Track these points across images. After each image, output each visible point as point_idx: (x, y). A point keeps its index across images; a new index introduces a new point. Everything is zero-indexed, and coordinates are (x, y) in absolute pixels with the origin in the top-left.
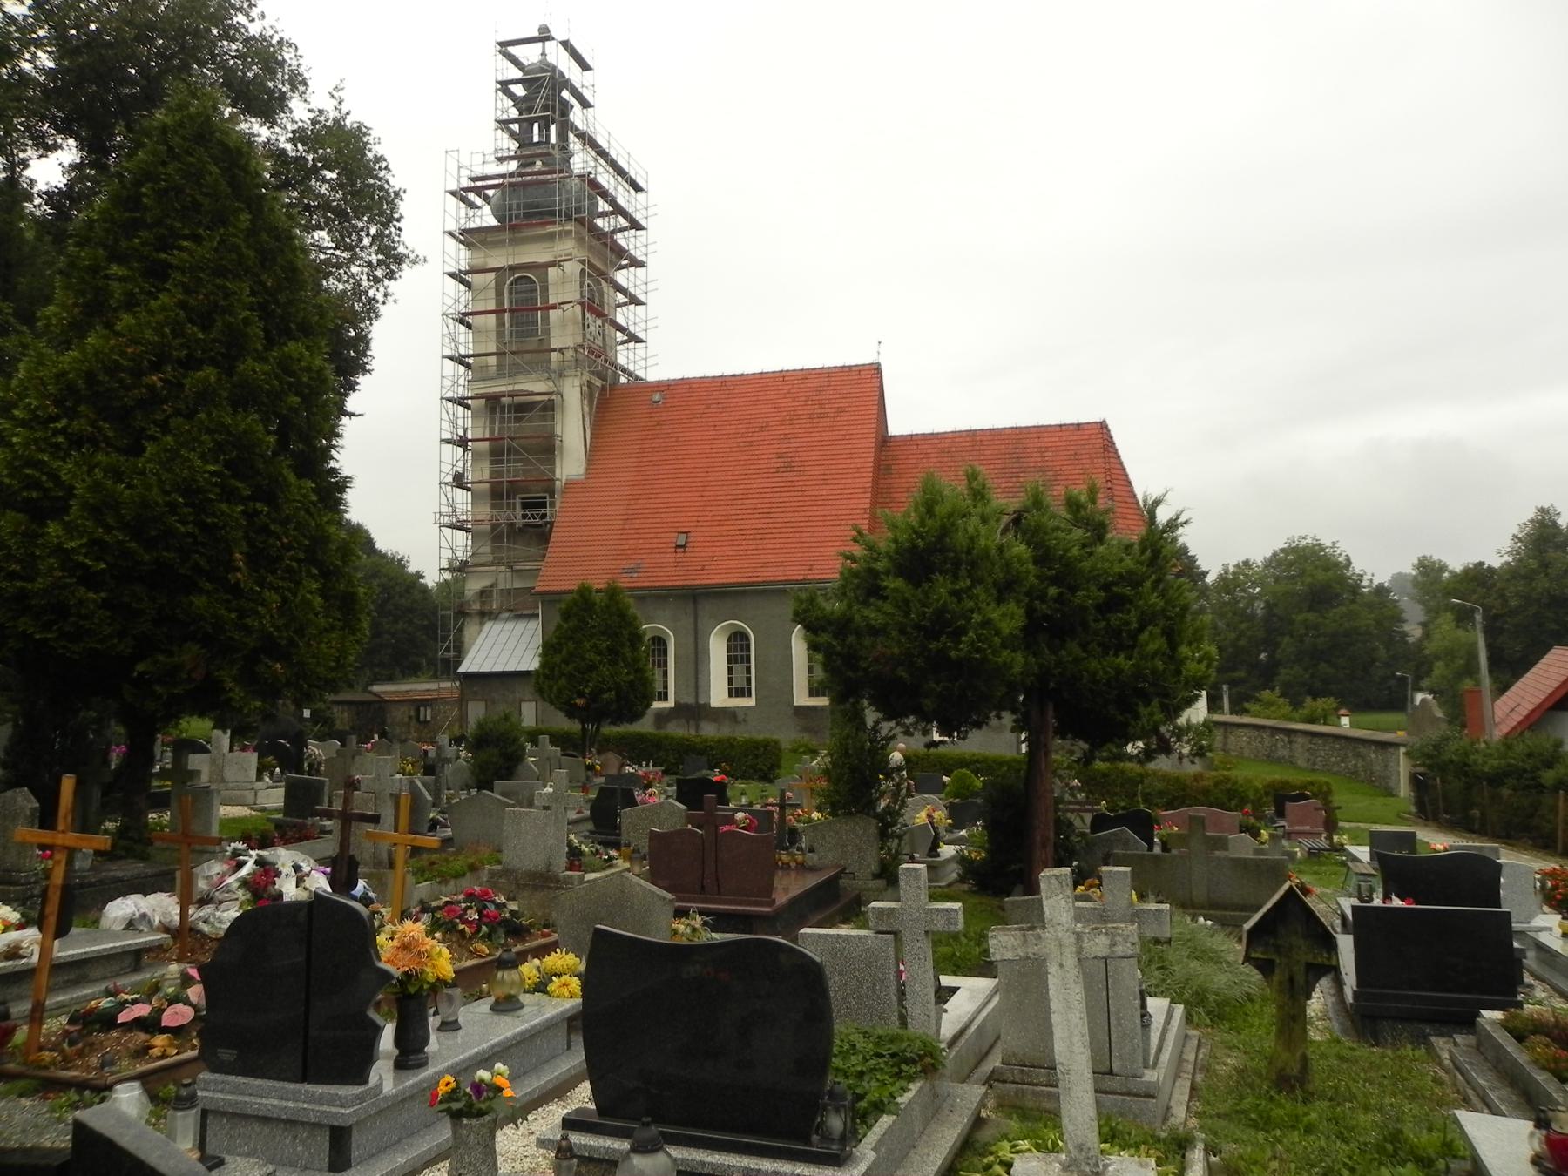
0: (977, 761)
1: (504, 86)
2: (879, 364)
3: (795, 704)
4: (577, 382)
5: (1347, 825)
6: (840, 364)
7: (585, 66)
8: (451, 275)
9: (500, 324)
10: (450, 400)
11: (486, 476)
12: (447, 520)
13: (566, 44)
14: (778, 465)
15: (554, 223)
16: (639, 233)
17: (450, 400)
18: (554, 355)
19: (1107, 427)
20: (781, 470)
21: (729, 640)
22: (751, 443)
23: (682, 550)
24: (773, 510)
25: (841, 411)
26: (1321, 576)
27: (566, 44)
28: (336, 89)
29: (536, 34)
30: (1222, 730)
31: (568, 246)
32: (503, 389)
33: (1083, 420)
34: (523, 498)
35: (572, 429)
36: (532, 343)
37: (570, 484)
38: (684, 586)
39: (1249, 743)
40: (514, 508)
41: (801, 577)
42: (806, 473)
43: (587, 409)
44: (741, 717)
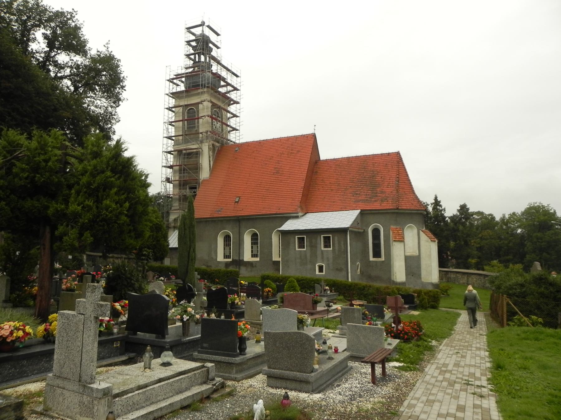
0: (303, 280)
1: (188, 43)
2: (315, 134)
3: (273, 260)
4: (207, 144)
5: (444, 309)
6: (301, 134)
7: (218, 34)
8: (167, 109)
9: (184, 125)
10: (165, 152)
11: (177, 178)
13: (208, 26)
15: (199, 89)
16: (238, 91)
17: (165, 152)
18: (201, 135)
19: (399, 154)
21: (252, 236)
25: (299, 151)
26: (542, 218)
27: (208, 26)
28: (107, 44)
29: (200, 23)
30: (466, 276)
31: (206, 97)
32: (182, 148)
33: (391, 152)
35: (205, 162)
36: (194, 131)
37: (204, 181)
39: (476, 281)
40: (186, 189)
43: (211, 153)
44: (254, 265)
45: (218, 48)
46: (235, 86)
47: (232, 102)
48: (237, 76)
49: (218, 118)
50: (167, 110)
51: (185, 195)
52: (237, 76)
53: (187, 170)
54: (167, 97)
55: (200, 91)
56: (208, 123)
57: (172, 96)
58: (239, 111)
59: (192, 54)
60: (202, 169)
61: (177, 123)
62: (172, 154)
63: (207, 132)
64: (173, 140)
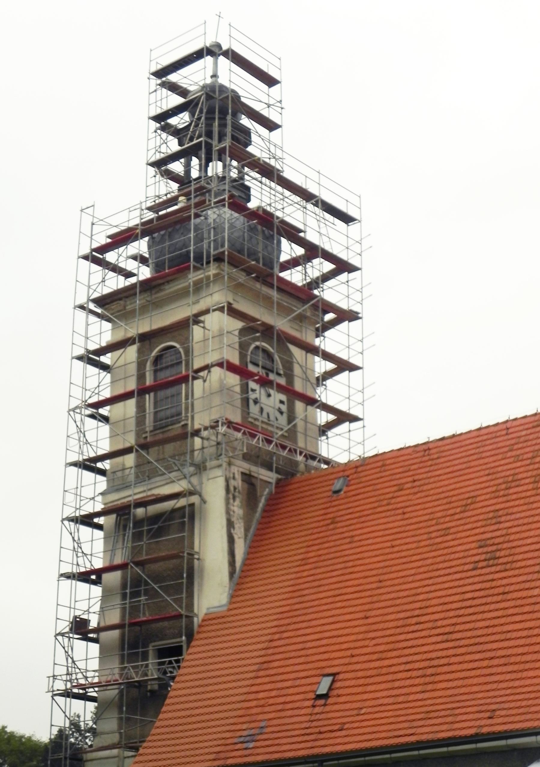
7: (270, 81)
8: (80, 358)
12: (60, 685)
14: (477, 558)
20: (481, 564)
22: (446, 532)
23: (322, 702)
24: (458, 628)
34: (153, 646)
37: (209, 619)
38: (308, 756)
40: (145, 657)
41: (472, 731)
42: (514, 565)
43: (238, 510)
45: (271, 126)
46: (343, 256)
47: (330, 316)
48: (347, 219)
49: (272, 377)
50: (80, 364)
51: (140, 685)
52: (347, 219)
53: (147, 584)
54: (81, 315)
55: (193, 277)
56: (223, 389)
57: (99, 311)
58: (358, 347)
59: (174, 157)
60: (201, 577)
61: (119, 407)
62: (99, 527)
63: (214, 426)
64: (102, 472)
